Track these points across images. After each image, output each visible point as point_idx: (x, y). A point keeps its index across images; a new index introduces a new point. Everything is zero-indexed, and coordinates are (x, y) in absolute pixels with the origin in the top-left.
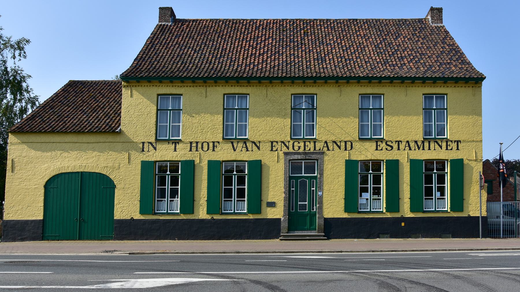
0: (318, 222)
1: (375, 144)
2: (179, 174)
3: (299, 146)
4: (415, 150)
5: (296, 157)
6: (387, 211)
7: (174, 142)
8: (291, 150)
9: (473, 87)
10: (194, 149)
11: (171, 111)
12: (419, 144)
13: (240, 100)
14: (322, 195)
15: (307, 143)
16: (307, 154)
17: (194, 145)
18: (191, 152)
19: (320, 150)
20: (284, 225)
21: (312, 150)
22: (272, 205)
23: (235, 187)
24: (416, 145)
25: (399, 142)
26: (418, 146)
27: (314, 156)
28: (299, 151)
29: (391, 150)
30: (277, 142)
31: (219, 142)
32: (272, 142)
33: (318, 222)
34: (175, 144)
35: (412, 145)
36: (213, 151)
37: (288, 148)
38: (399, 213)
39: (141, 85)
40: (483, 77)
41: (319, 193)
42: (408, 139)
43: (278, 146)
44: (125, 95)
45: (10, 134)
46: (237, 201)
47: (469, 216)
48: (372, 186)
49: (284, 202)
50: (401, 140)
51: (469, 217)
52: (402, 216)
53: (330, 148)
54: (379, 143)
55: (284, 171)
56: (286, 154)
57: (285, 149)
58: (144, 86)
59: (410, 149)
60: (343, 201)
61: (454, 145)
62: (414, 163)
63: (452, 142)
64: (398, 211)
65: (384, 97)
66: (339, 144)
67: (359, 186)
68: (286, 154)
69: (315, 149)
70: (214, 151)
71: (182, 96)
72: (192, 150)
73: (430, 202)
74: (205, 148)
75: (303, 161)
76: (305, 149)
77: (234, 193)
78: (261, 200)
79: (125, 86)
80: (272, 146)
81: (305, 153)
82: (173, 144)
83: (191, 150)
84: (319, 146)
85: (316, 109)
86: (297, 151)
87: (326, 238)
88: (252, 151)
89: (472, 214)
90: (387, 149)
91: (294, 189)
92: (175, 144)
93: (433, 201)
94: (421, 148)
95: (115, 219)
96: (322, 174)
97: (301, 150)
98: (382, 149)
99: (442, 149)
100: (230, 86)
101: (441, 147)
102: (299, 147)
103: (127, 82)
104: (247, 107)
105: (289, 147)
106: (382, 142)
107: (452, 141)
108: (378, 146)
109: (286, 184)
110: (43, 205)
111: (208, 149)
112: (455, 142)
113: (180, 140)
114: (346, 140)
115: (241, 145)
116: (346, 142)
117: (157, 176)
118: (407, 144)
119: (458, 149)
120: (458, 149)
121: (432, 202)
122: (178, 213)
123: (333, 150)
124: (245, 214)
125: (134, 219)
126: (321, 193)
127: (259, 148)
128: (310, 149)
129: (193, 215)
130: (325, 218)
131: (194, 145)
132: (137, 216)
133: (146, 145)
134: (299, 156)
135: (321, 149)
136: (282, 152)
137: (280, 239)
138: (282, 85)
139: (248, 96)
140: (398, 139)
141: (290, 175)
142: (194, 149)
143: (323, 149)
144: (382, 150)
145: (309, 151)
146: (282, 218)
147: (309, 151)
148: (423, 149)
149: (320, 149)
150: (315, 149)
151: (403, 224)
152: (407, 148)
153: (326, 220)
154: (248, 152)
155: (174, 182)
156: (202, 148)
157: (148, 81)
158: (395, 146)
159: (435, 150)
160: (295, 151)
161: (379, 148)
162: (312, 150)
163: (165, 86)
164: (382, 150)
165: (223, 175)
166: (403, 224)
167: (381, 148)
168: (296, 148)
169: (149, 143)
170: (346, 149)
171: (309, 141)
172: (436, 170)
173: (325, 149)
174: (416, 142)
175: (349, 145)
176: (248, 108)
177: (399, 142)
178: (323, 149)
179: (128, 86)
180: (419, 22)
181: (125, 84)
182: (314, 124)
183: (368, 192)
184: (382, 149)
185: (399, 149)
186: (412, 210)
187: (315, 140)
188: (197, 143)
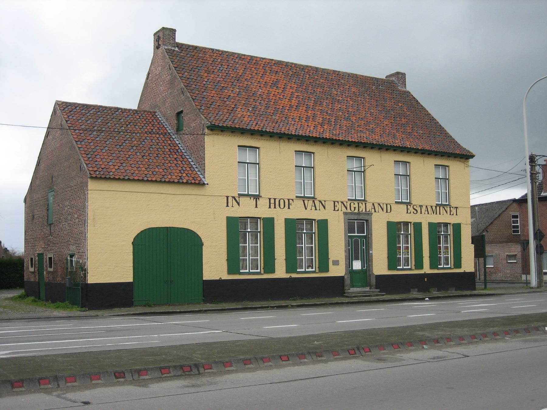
1: (406, 206)
3: (354, 207)
4: (431, 214)
6: (264, 273)
8: (349, 211)
10: (272, 206)
19: (369, 211)
22: (336, 263)
31: (293, 200)
32: (334, 202)
36: (274, 208)
38: (329, 273)
40: (474, 155)
43: (339, 206)
44: (207, 144)
47: (291, 277)
51: (465, 273)
52: (220, 278)
56: (345, 214)
60: (284, 262)
65: (261, 154)
70: (290, 209)
72: (271, 207)
75: (356, 221)
76: (359, 211)
81: (359, 214)
83: (270, 207)
87: (385, 293)
88: (320, 210)
89: (468, 270)
94: (435, 213)
97: (356, 211)
99: (239, 206)
103: (212, 130)
104: (407, 174)
106: (410, 206)
115: (311, 202)
124: (450, 268)
129: (275, 274)
131: (272, 201)
132: (225, 276)
135: (370, 211)
140: (421, 204)
142: (272, 206)
148: (436, 214)
151: (426, 279)
154: (316, 211)
160: (351, 212)
166: (426, 279)
168: (353, 209)
172: (305, 230)
173: (373, 210)
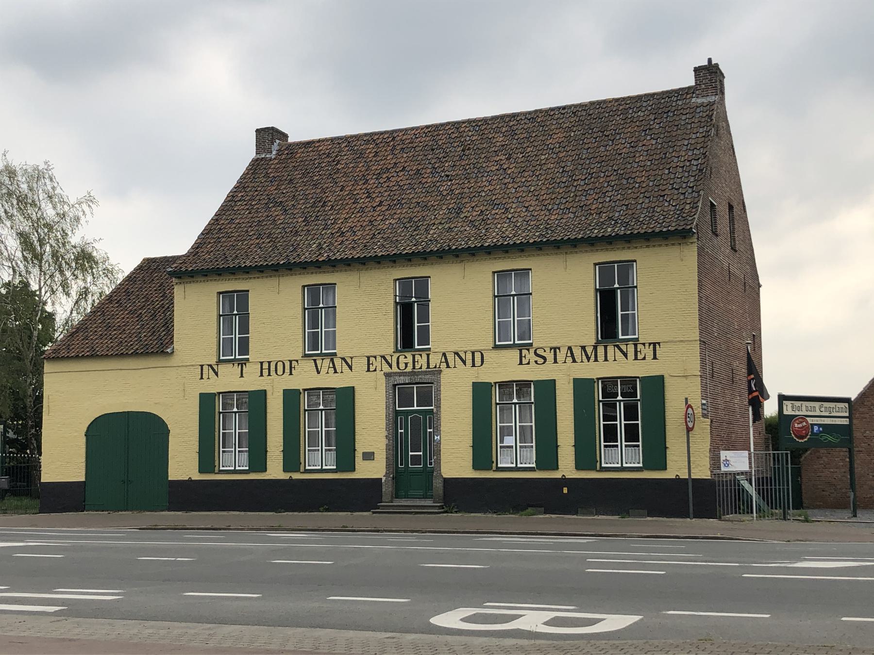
0: (438, 484)
2: (639, 400)
4: (582, 362)
5: (401, 380)
7: (240, 363)
8: (395, 369)
9: (680, 244)
10: (265, 372)
11: (516, 298)
12: (589, 350)
13: (325, 292)
14: (440, 441)
15: (524, 352)
16: (417, 375)
17: (266, 366)
18: (262, 378)
19: (435, 367)
20: (387, 489)
21: (424, 368)
22: (369, 456)
23: (621, 423)
24: (583, 354)
25: (555, 349)
26: (587, 355)
27: (427, 378)
28: (405, 371)
29: (544, 363)
30: (375, 357)
31: (297, 361)
32: (368, 358)
33: (438, 484)
34: (242, 364)
35: (577, 352)
37: (391, 366)
38: (666, 471)
39: (640, 245)
41: (436, 438)
42: (570, 345)
43: (377, 363)
45: (45, 361)
46: (626, 446)
48: (618, 422)
49: (387, 452)
50: (558, 345)
53: (450, 364)
54: (524, 352)
55: (386, 402)
56: (387, 375)
57: (386, 368)
58: (201, 281)
59: (574, 361)
61: (649, 351)
62: (582, 387)
63: (644, 346)
64: (664, 468)
66: (349, 361)
67: (639, 422)
68: (387, 375)
69: (428, 367)
71: (429, 279)
73: (630, 450)
74: (280, 371)
77: (621, 433)
78: (355, 450)
79: (177, 283)
80: (369, 364)
82: (238, 365)
83: (262, 375)
84: (435, 360)
85: (220, 316)
86: (404, 371)
90: (536, 362)
91: (403, 431)
92: (242, 364)
93: (639, 449)
94: (593, 358)
95: (169, 479)
96: (438, 407)
98: (529, 362)
100: (306, 273)
101: (625, 355)
102: (406, 364)
105: (391, 365)
106: (529, 351)
107: (644, 344)
108: (523, 358)
109: (389, 424)
110: (84, 461)
111: (284, 372)
112: (649, 346)
113: (247, 360)
114: (473, 349)
115: (327, 362)
116: (473, 353)
117: (601, 404)
118: (569, 352)
119: (655, 358)
120: (655, 358)
121: (637, 451)
122: (534, 468)
123: (455, 367)
125: (191, 480)
126: (439, 437)
127: (350, 368)
128: (421, 366)
130: (445, 479)
131: (266, 366)
132: (197, 476)
133: (205, 368)
134: (407, 378)
135: (438, 366)
136: (382, 372)
137: (372, 512)
138: (379, 267)
139: (530, 271)
140: (554, 345)
141: (397, 409)
142: (265, 372)
143: (440, 365)
144: (528, 363)
145: (420, 370)
146: (383, 477)
147: (420, 370)
149: (436, 366)
150: (428, 367)
151: (565, 490)
152: (570, 359)
153: (446, 481)
155: (630, 412)
156: (276, 370)
157: (390, 260)
158: (550, 356)
159: (615, 360)
161: (525, 361)
162: (424, 368)
163: (226, 279)
164: (528, 363)
165: (599, 401)
166: (565, 490)
167: (643, 356)
168: (402, 366)
169: (209, 365)
170: (474, 365)
171: (420, 353)
172: (621, 396)
174: (583, 348)
175: (478, 356)
176: (635, 285)
177: (654, 344)
178: (440, 365)
179: (180, 283)
180: (19, 201)
181: (177, 281)
182: (530, 320)
183: (512, 436)
184: (529, 362)
185: (555, 362)
186: (579, 467)
187: (428, 352)
188: (269, 363)
